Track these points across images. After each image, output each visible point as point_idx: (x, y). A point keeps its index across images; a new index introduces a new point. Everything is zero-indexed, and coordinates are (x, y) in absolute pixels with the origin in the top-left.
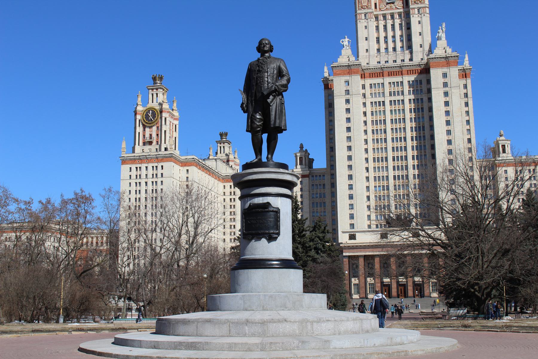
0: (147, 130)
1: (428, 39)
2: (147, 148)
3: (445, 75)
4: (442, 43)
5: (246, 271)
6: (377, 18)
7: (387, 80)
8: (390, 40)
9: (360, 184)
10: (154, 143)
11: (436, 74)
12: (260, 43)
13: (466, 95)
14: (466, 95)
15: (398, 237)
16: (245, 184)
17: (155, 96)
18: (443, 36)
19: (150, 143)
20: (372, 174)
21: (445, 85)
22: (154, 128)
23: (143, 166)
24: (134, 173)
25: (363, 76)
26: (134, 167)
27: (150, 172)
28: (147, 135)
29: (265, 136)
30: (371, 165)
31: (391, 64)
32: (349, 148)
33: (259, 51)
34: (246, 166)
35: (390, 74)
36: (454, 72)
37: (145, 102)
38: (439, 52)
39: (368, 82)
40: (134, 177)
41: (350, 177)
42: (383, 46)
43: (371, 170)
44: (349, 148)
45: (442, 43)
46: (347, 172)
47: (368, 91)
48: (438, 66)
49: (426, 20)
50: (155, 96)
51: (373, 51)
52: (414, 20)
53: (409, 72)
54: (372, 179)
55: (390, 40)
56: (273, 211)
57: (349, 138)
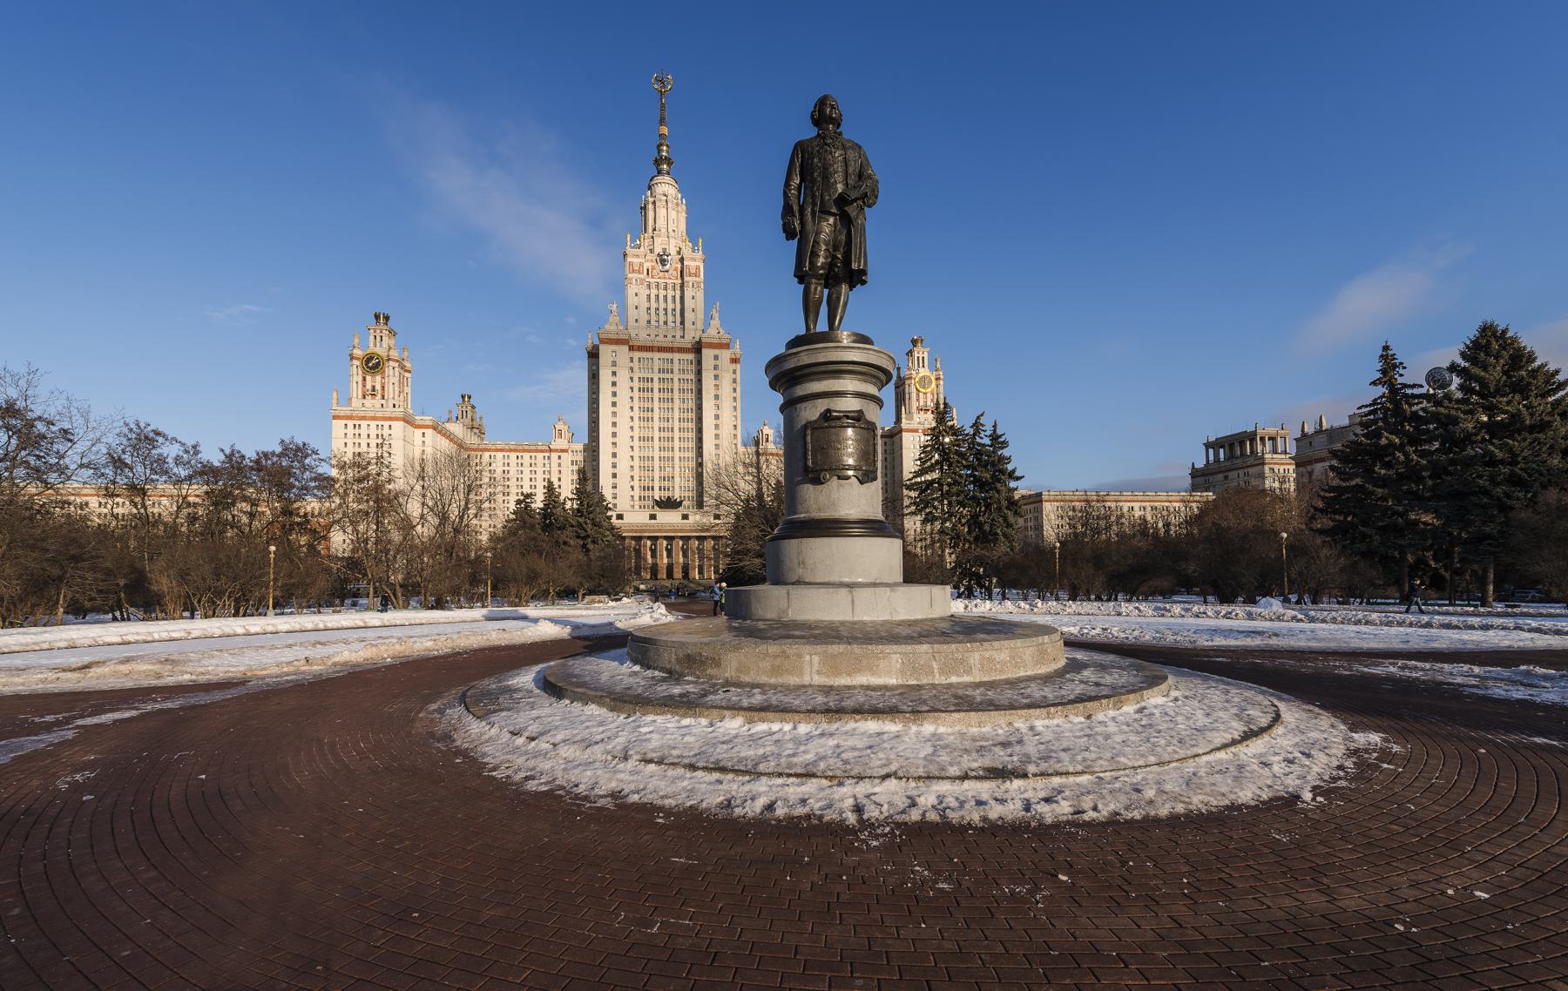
1: (701, 315)
2: (369, 401)
3: (716, 358)
4: (716, 322)
5: (794, 541)
6: (649, 286)
7: (657, 355)
8: (662, 312)
9: (623, 464)
11: (707, 354)
12: (822, 102)
13: (735, 381)
14: (735, 381)
15: (669, 519)
16: (787, 376)
18: (716, 316)
20: (636, 454)
21: (716, 367)
22: (378, 378)
23: (364, 424)
24: (350, 430)
25: (632, 348)
26: (350, 423)
27: (373, 432)
28: (369, 386)
30: (636, 443)
31: (661, 338)
32: (614, 424)
33: (816, 123)
34: (797, 342)
35: (661, 349)
36: (726, 355)
38: (712, 332)
39: (637, 355)
40: (350, 435)
41: (614, 455)
42: (654, 317)
43: (636, 448)
44: (614, 424)
45: (716, 322)
46: (611, 450)
47: (636, 365)
48: (711, 346)
49: (700, 295)
51: (643, 323)
52: (688, 293)
53: (680, 350)
54: (636, 459)
55: (662, 312)
57: (614, 414)
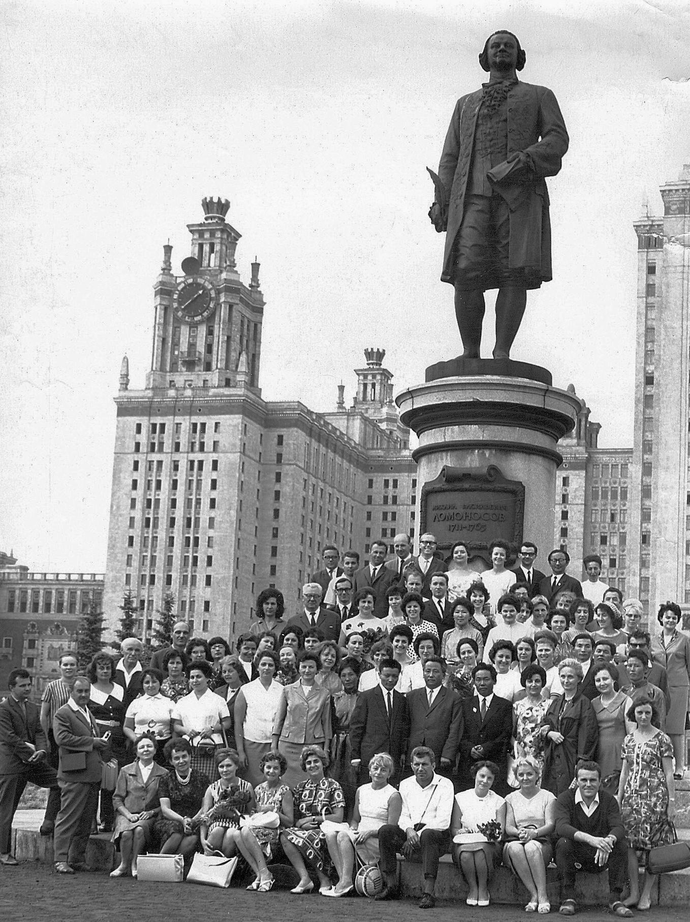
29: (491, 296)
56: (505, 491)
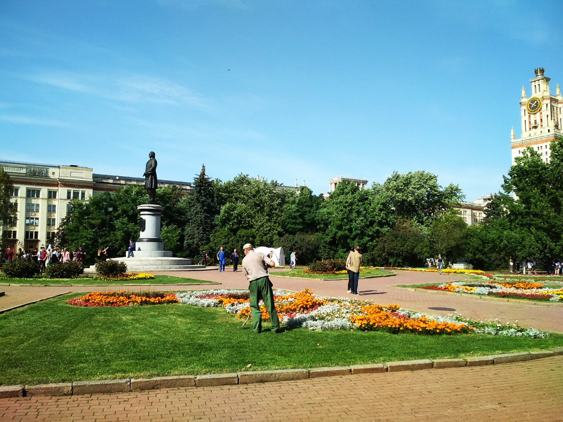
0: (532, 116)
10: (539, 127)
17: (537, 86)
19: (535, 127)
22: (538, 114)
28: (533, 122)
37: (529, 93)
50: (537, 86)
